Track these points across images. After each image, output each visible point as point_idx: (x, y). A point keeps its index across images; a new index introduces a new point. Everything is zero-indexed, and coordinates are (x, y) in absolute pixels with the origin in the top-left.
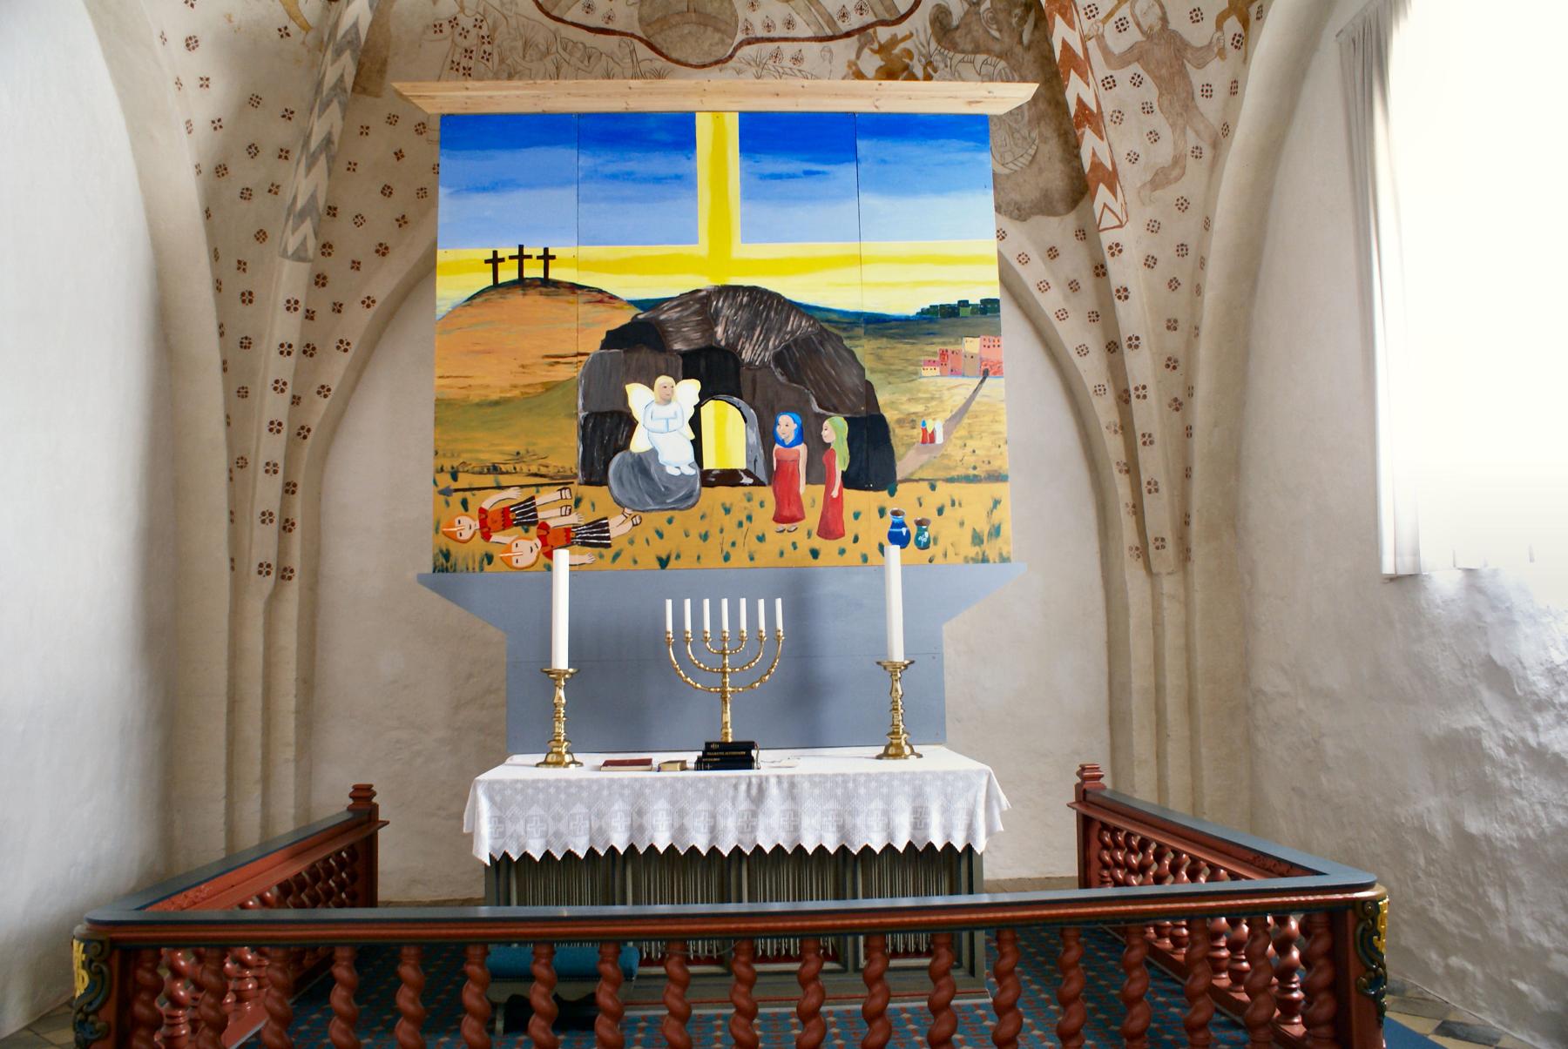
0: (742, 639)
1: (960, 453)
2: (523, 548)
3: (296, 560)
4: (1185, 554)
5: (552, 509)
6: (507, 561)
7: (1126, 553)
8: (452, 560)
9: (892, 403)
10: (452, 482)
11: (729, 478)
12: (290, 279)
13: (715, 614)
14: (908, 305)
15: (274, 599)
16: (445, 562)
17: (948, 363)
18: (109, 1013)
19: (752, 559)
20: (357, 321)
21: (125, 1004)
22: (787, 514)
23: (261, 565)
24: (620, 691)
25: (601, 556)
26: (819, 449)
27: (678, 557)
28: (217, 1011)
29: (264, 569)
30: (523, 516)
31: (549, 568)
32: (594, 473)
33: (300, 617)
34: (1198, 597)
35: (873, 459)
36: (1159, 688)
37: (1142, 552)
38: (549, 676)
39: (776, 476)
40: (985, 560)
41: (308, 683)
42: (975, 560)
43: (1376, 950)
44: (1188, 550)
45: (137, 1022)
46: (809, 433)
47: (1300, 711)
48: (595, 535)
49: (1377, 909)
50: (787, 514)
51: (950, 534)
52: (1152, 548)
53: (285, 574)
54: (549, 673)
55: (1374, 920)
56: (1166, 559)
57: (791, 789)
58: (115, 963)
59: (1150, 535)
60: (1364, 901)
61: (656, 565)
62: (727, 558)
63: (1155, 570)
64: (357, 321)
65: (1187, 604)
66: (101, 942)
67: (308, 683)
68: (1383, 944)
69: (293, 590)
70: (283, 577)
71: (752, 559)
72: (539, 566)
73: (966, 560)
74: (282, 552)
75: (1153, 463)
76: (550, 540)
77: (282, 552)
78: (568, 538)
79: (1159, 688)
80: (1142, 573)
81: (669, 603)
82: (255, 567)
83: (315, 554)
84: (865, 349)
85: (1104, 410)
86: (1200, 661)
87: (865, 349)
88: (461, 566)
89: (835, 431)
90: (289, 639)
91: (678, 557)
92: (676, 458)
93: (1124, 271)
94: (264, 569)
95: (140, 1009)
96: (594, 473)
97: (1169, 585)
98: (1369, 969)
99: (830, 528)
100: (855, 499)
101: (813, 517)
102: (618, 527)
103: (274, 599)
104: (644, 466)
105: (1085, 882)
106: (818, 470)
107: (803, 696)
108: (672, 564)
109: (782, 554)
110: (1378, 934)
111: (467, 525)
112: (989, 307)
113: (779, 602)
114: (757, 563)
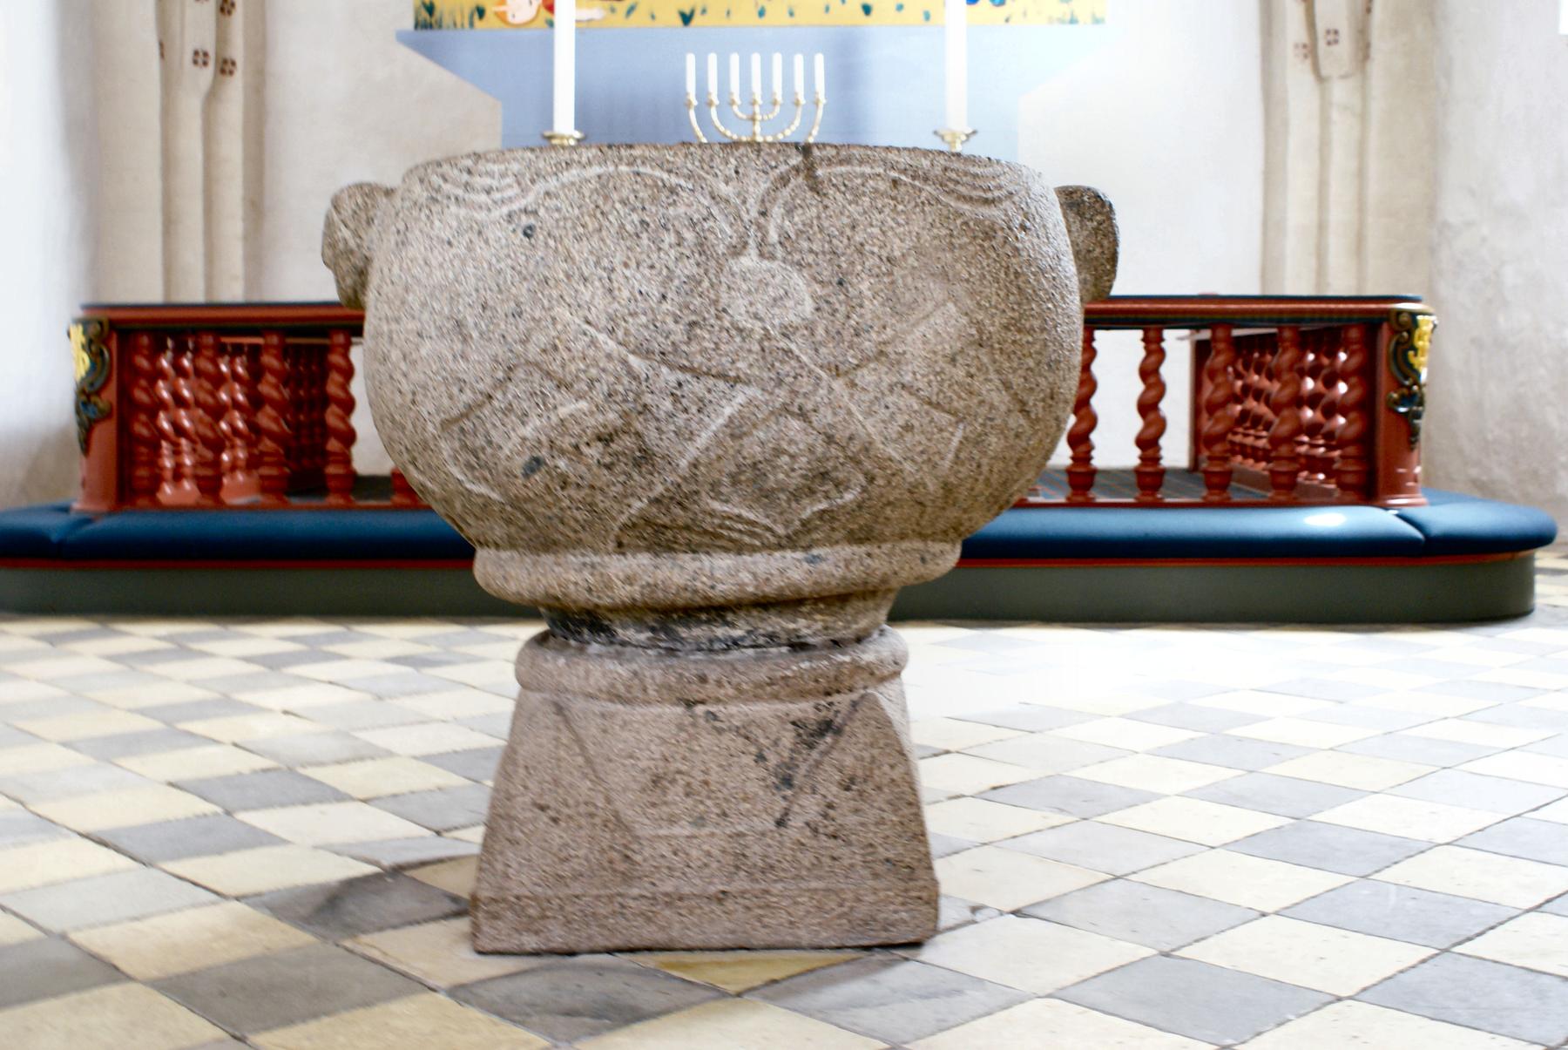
0: (775, 103)
3: (237, 52)
4: (1363, 50)
6: (502, 17)
7: (1290, 51)
8: (437, 13)
15: (212, 97)
18: (110, 395)
19: (791, 14)
21: (124, 394)
23: (196, 53)
25: (613, 10)
27: (704, 11)
28: (213, 430)
29: (200, 58)
31: (551, 24)
33: (246, 114)
34: (1377, 108)
36: (1322, 227)
37: (1310, 51)
40: (1073, 21)
42: (1061, 21)
43: (1411, 366)
44: (1367, 46)
45: (138, 407)
47: (1484, 240)
49: (1415, 324)
52: (1322, 44)
53: (225, 67)
54: (550, 138)
55: (1411, 333)
56: (1339, 57)
58: (114, 344)
59: (1321, 27)
60: (1400, 312)
61: (679, 21)
62: (762, 13)
63: (1324, 72)
65: (1363, 117)
66: (101, 324)
68: (1423, 366)
69: (236, 86)
70: (223, 71)
71: (791, 14)
72: (541, 23)
73: (1050, 20)
74: (222, 38)
77: (222, 38)
79: (1322, 227)
80: (1309, 77)
81: (691, 60)
82: (189, 57)
83: (260, 47)
86: (1374, 190)
88: (447, 21)
90: (232, 149)
91: (704, 11)
94: (200, 58)
95: (140, 396)
97: (1341, 92)
98: (1402, 386)
103: (212, 97)
105: (1214, 480)
108: (697, 20)
109: (827, 9)
110: (1415, 349)
113: (819, 60)
114: (796, 20)
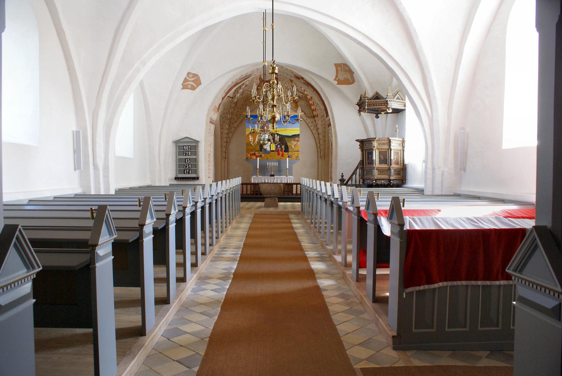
1: (296, 149)
2: (254, 157)
5: (257, 154)
9: (288, 144)
10: (248, 151)
11: (273, 151)
12: (227, 126)
13: (272, 164)
14: (290, 134)
16: (247, 158)
17: (294, 140)
20: (233, 129)
22: (279, 154)
24: (264, 170)
26: (282, 149)
30: (254, 154)
32: (261, 150)
35: (287, 150)
38: (257, 169)
39: (278, 151)
41: (228, 170)
46: (281, 147)
48: (261, 156)
50: (279, 154)
51: (294, 157)
56: (323, 158)
57: (277, 178)
64: (233, 129)
67: (228, 170)
75: (322, 147)
76: (257, 157)
78: (258, 156)
84: (286, 139)
85: (317, 141)
87: (286, 139)
89: (283, 147)
92: (268, 149)
93: (319, 126)
96: (261, 150)
99: (282, 156)
100: (285, 153)
101: (281, 155)
102: (263, 155)
104: (265, 150)
106: (282, 150)
107: (279, 171)
111: (249, 155)
112: (299, 135)
